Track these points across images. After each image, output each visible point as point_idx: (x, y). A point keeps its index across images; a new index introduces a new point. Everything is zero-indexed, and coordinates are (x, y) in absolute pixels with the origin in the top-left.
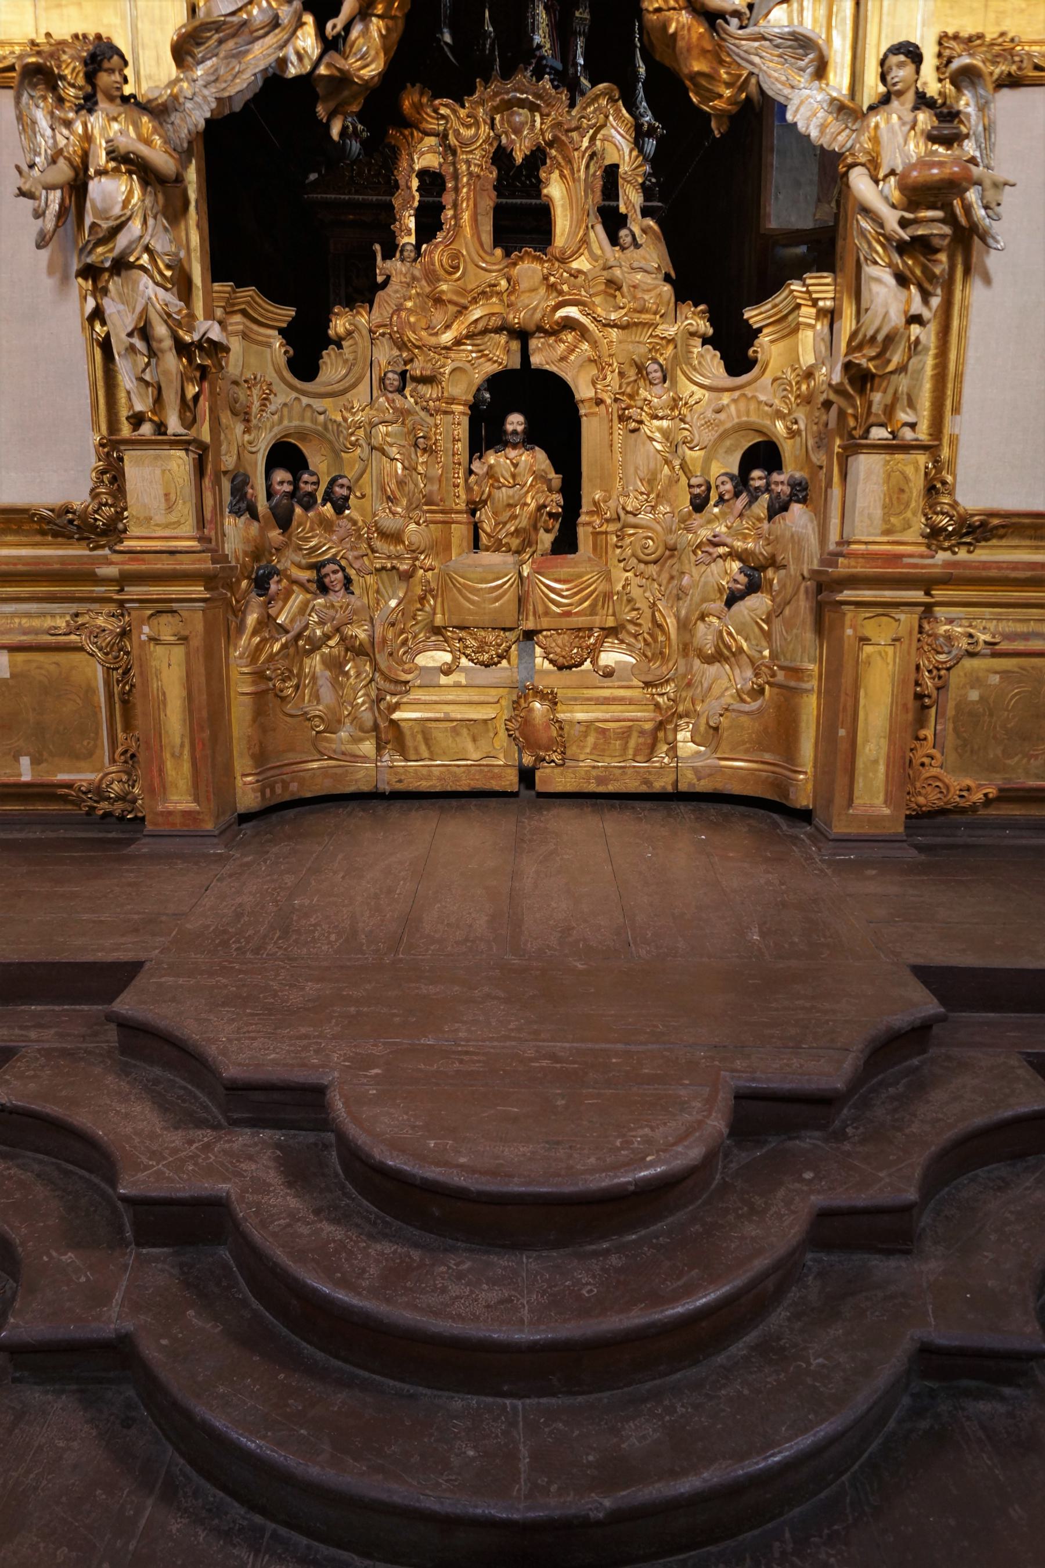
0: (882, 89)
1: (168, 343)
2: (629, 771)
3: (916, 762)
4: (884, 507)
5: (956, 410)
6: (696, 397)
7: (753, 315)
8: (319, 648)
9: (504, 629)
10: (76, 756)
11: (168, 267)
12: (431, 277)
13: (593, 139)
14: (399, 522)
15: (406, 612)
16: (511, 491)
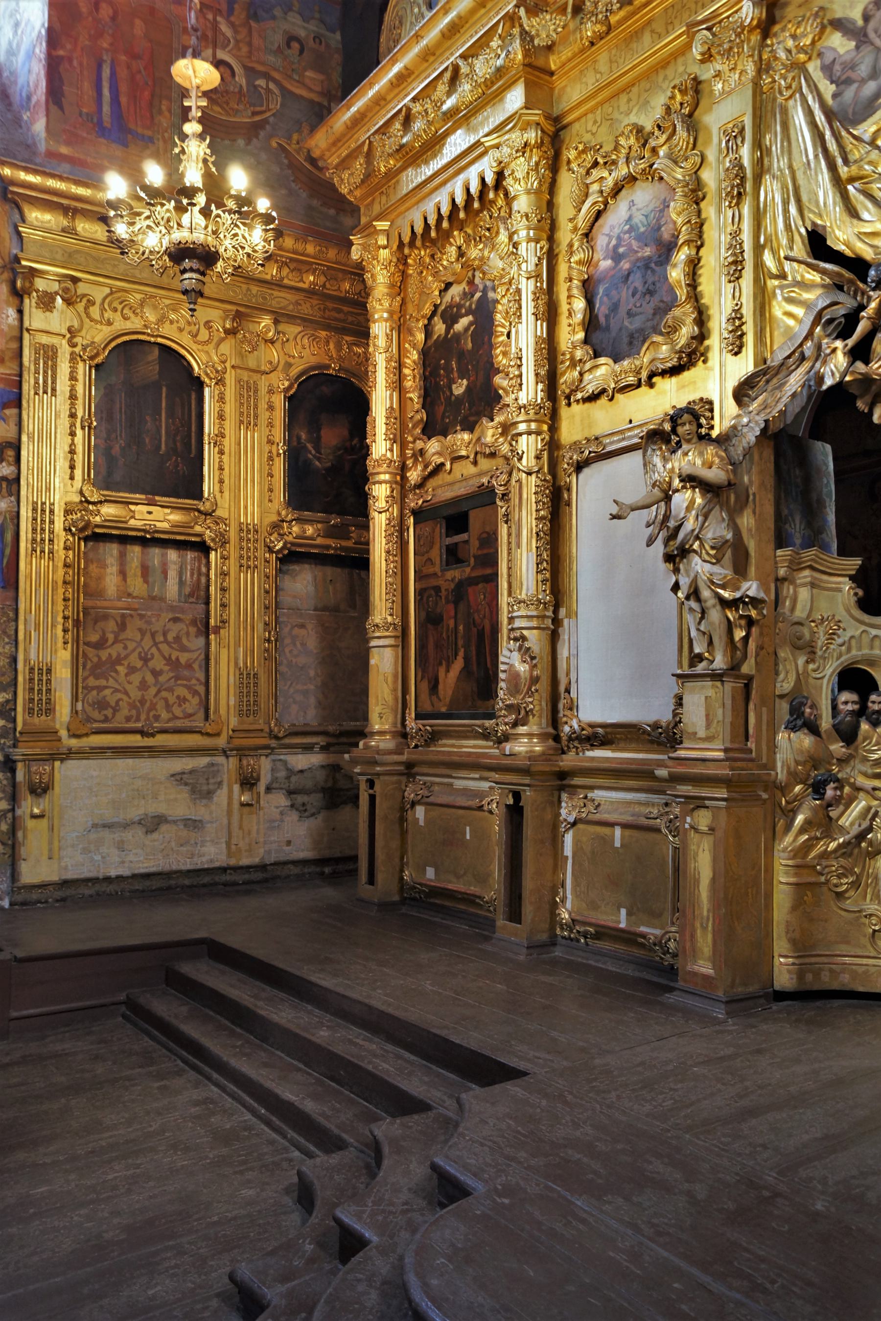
11: (712, 548)
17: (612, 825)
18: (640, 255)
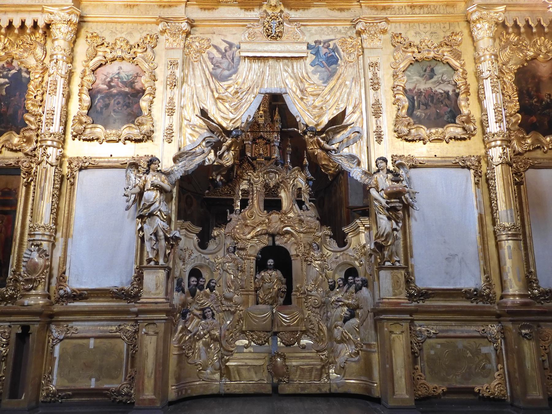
0: (377, 168)
1: (163, 237)
2: (313, 385)
3: (416, 378)
4: (393, 287)
5: (412, 257)
6: (329, 254)
7: (346, 229)
8: (202, 339)
9: (267, 332)
10: (113, 378)
11: (165, 215)
12: (244, 219)
13: (294, 181)
14: (231, 294)
15: (232, 325)
16: (269, 284)
17: (89, 338)
18: (123, 89)
